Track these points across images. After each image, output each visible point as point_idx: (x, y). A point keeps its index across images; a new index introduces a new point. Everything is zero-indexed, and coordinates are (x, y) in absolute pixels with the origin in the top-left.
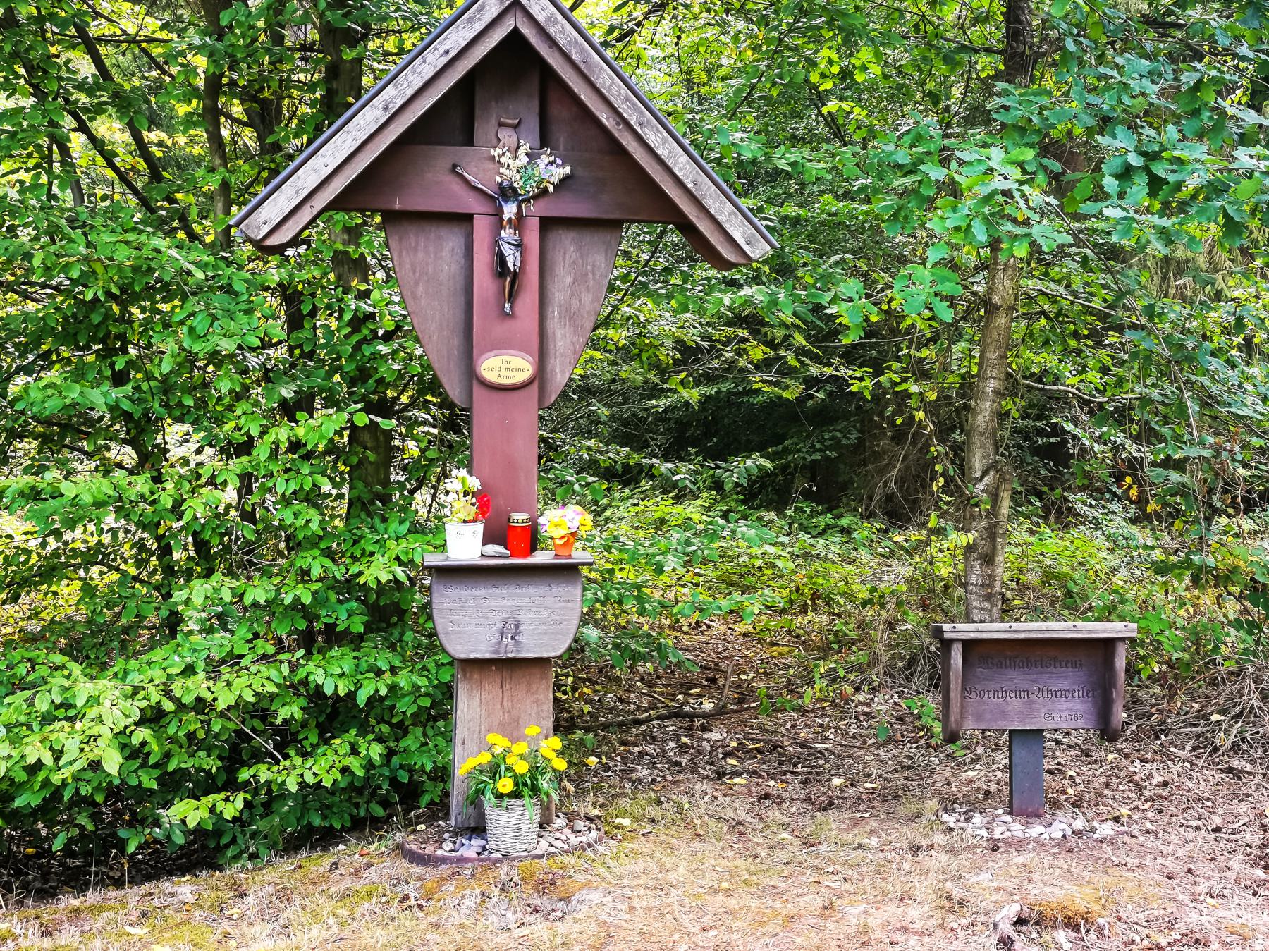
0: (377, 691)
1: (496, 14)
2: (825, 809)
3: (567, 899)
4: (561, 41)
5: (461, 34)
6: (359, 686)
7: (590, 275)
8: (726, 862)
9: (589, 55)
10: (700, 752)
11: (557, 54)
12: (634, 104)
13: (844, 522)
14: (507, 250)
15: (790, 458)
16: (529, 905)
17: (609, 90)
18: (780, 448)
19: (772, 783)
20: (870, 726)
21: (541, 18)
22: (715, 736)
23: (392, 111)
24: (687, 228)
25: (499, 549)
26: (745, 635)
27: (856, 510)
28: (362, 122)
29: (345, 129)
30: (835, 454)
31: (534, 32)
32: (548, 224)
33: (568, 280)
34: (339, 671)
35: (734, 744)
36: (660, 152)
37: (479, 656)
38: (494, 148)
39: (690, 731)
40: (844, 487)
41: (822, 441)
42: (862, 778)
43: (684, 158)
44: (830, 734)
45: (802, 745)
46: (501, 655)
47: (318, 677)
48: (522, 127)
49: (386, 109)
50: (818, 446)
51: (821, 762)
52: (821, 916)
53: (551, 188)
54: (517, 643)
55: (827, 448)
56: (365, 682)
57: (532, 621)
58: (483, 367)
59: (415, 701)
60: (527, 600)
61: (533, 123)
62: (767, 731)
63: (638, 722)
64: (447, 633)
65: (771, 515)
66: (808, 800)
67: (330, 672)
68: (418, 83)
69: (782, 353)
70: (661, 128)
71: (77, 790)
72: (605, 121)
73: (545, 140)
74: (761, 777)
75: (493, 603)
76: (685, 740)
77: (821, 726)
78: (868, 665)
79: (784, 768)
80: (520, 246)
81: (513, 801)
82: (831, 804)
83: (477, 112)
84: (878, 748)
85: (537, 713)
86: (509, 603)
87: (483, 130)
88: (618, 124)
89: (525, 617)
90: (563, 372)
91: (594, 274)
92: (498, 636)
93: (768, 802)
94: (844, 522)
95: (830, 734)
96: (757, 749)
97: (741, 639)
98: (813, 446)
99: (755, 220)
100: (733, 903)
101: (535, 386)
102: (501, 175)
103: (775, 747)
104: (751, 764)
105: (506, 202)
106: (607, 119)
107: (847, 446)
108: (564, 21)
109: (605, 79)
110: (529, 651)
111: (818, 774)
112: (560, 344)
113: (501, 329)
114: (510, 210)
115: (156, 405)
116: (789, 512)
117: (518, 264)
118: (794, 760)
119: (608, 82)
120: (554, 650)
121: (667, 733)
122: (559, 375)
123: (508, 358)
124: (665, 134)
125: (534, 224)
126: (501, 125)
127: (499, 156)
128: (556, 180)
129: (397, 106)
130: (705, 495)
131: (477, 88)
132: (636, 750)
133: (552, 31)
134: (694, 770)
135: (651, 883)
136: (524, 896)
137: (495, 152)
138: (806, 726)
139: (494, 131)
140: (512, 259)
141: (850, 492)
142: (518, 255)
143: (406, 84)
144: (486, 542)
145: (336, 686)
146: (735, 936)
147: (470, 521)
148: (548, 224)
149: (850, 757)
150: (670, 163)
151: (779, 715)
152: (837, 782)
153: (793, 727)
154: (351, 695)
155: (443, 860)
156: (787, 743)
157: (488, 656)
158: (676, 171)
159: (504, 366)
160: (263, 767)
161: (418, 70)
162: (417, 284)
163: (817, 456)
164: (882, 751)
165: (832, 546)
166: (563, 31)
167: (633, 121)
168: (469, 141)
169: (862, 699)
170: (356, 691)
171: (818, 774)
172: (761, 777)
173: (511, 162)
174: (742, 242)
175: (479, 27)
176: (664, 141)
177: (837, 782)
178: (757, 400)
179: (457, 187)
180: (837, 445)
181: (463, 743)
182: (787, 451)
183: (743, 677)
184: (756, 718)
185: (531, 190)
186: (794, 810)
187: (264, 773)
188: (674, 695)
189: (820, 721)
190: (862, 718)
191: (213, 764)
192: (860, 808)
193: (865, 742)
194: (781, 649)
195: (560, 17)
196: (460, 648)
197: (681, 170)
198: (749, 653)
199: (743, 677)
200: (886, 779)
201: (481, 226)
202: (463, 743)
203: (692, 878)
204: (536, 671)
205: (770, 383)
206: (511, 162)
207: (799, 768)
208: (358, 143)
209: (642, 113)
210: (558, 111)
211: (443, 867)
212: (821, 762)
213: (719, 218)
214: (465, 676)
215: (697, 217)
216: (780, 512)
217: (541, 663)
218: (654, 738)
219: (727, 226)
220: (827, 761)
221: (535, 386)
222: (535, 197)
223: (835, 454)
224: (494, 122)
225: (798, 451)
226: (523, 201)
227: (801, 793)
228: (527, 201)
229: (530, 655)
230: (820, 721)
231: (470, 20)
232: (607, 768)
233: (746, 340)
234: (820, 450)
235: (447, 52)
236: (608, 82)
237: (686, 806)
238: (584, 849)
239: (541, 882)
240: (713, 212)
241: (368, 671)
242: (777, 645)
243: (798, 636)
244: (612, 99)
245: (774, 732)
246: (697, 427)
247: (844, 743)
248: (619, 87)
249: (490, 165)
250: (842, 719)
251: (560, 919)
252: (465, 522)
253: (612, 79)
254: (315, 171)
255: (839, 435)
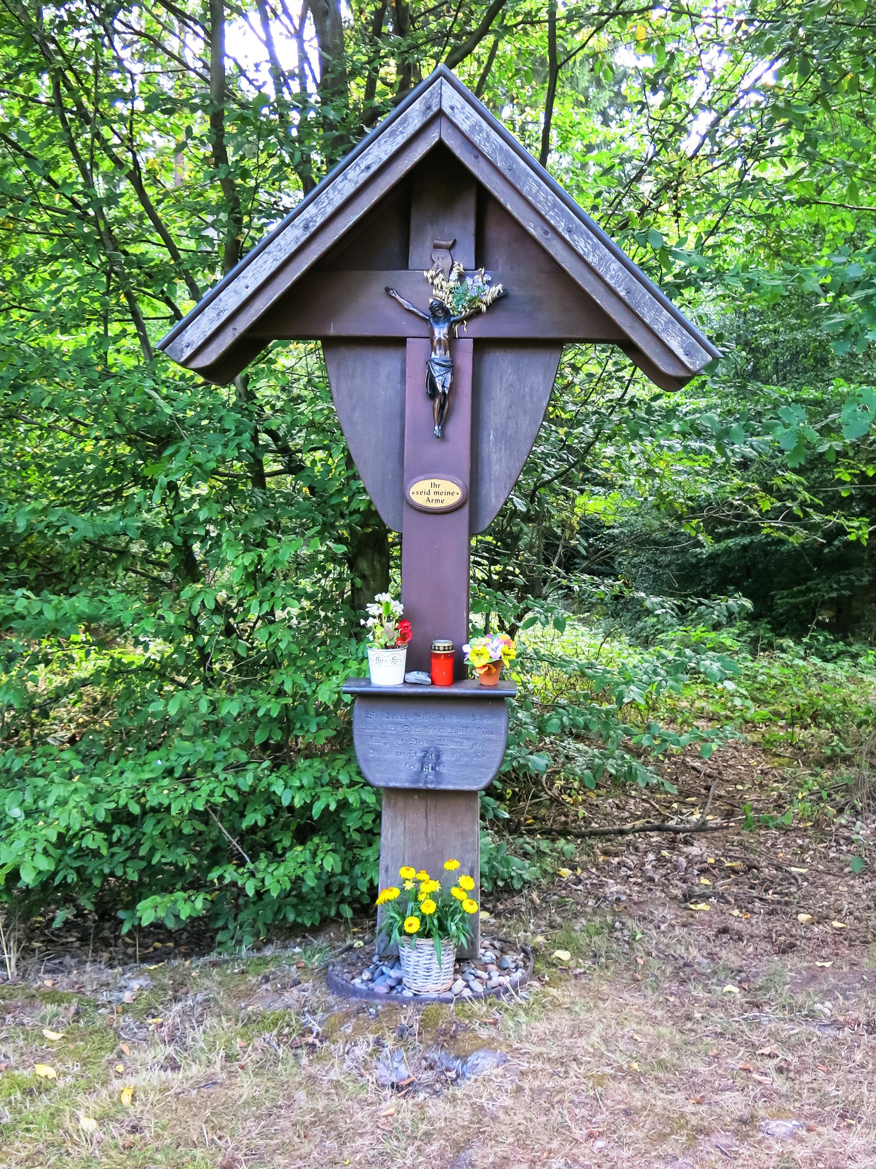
0: (328, 806)
1: (419, 125)
2: (784, 952)
3: (463, 1058)
4: (486, 149)
5: (383, 148)
6: (315, 798)
7: (528, 398)
8: (648, 1028)
9: (515, 161)
10: (676, 868)
11: (483, 163)
12: (562, 210)
13: (854, 649)
14: (437, 370)
15: (811, 595)
16: (426, 1059)
17: (536, 197)
18: (803, 587)
19: (736, 912)
20: (849, 851)
21: (465, 127)
22: (694, 850)
23: (313, 229)
24: (630, 348)
25: (422, 677)
26: (754, 744)
27: (866, 639)
28: (283, 242)
29: (267, 250)
30: (848, 593)
31: (459, 142)
32: (482, 345)
33: (504, 403)
34: (298, 784)
35: (711, 860)
36: (590, 259)
37: (398, 785)
38: (428, 270)
39: (672, 845)
40: (858, 619)
41: (838, 582)
42: (833, 914)
43: (616, 265)
44: (807, 858)
45: (778, 868)
46: (421, 785)
47: (278, 788)
48: (457, 248)
49: (306, 227)
50: (835, 586)
51: (793, 889)
52: (736, 1133)
53: (484, 308)
54: (438, 774)
55: (843, 588)
56: (322, 795)
57: (454, 751)
58: (413, 489)
59: (361, 818)
60: (449, 730)
61: (468, 244)
62: (746, 848)
63: (622, 833)
64: (367, 760)
65: (788, 642)
66: (768, 938)
67: (290, 783)
68: (338, 200)
69: (788, 504)
70: (591, 235)
71: (65, 877)
72: (532, 231)
73: (481, 260)
74: (728, 902)
75: (416, 731)
76: (665, 853)
77: (801, 847)
78: (856, 785)
79: (754, 893)
80: (451, 367)
81: (423, 941)
82: (792, 946)
83: (413, 236)
84: (854, 878)
85: (462, 845)
86: (431, 732)
87: (415, 257)
88: (546, 233)
89: (447, 747)
90: (497, 497)
91: (531, 396)
92: (418, 766)
93: (725, 938)
94: (854, 649)
95: (807, 858)
96: (731, 868)
97: (750, 748)
98: (831, 587)
99: (713, 347)
100: (637, 1098)
101: (466, 510)
102: (432, 295)
103: (750, 868)
104: (721, 885)
105: (437, 323)
106: (534, 228)
107: (861, 587)
108: (489, 129)
109: (532, 186)
110: (450, 783)
111: (787, 903)
112: (495, 468)
113: (434, 450)
114: (440, 332)
115: (176, 534)
116: (805, 640)
117: (448, 385)
118: (767, 884)
119: (535, 188)
120: (476, 784)
121: (649, 843)
122: (493, 500)
123: (437, 482)
124: (595, 240)
125: (467, 346)
126: (437, 247)
127: (433, 278)
128: (488, 299)
129: (318, 224)
130: (739, 624)
131: (413, 212)
132: (617, 860)
133: (476, 139)
134: (664, 888)
135: (554, 1054)
136: (422, 1047)
137: (428, 274)
138: (786, 845)
139: (428, 253)
140: (442, 380)
141: (862, 624)
142: (449, 376)
143: (327, 201)
144: (408, 670)
145: (293, 798)
146: (626, 1153)
147: (393, 647)
148: (482, 345)
149: (824, 885)
150: (601, 271)
151: (763, 832)
152: (803, 917)
153: (773, 845)
154: (308, 807)
155: (355, 992)
156: (764, 864)
157: (407, 785)
158: (607, 279)
159: (433, 490)
160: (231, 868)
161: (339, 187)
162: (353, 409)
163: (834, 595)
164: (857, 882)
165: (838, 671)
166: (488, 138)
167: (561, 228)
168: (405, 266)
169: (843, 822)
170: (312, 803)
171: (787, 903)
172: (728, 902)
173: (444, 283)
174: (680, 352)
175: (401, 140)
176: (595, 247)
177: (803, 917)
178: (784, 548)
179: (390, 311)
180: (851, 585)
181: (387, 871)
182: (809, 590)
183: (740, 787)
184: (738, 834)
185: (461, 310)
186: (751, 950)
187: (230, 873)
188: (671, 802)
189: (800, 842)
190: (842, 842)
191: (187, 861)
192: (823, 953)
193: (842, 869)
194: (782, 761)
195: (485, 125)
196: (379, 779)
197: (612, 277)
198: (752, 762)
199: (740, 787)
200: (856, 918)
201: (415, 349)
202: (387, 871)
203: (603, 1048)
204: (462, 802)
205: (778, 529)
206: (444, 283)
207: (770, 896)
208: (277, 264)
209: (571, 219)
210: (495, 232)
211: (353, 999)
212: (793, 889)
213: (655, 327)
214: (389, 803)
215: (632, 327)
216: (798, 642)
217: (470, 795)
218: (636, 849)
219: (664, 336)
220: (799, 888)
221: (466, 510)
222: (469, 318)
223: (848, 593)
224: (429, 244)
225: (819, 590)
226: (456, 322)
227: (761, 929)
228: (460, 321)
229: (451, 787)
230: (800, 842)
231: (393, 134)
232: (579, 881)
233: (757, 491)
234: (836, 590)
235: (368, 168)
236: (535, 188)
237: (639, 936)
238: (498, 995)
239: (445, 1033)
240: (647, 321)
241: (327, 785)
242: (779, 756)
243: (800, 749)
244: (538, 206)
245: (753, 851)
246: (738, 571)
247: (821, 867)
248: (547, 193)
249: (424, 288)
250: (822, 841)
251: (454, 1081)
252: (386, 647)
253: (539, 185)
254: (236, 292)
255: (853, 578)
